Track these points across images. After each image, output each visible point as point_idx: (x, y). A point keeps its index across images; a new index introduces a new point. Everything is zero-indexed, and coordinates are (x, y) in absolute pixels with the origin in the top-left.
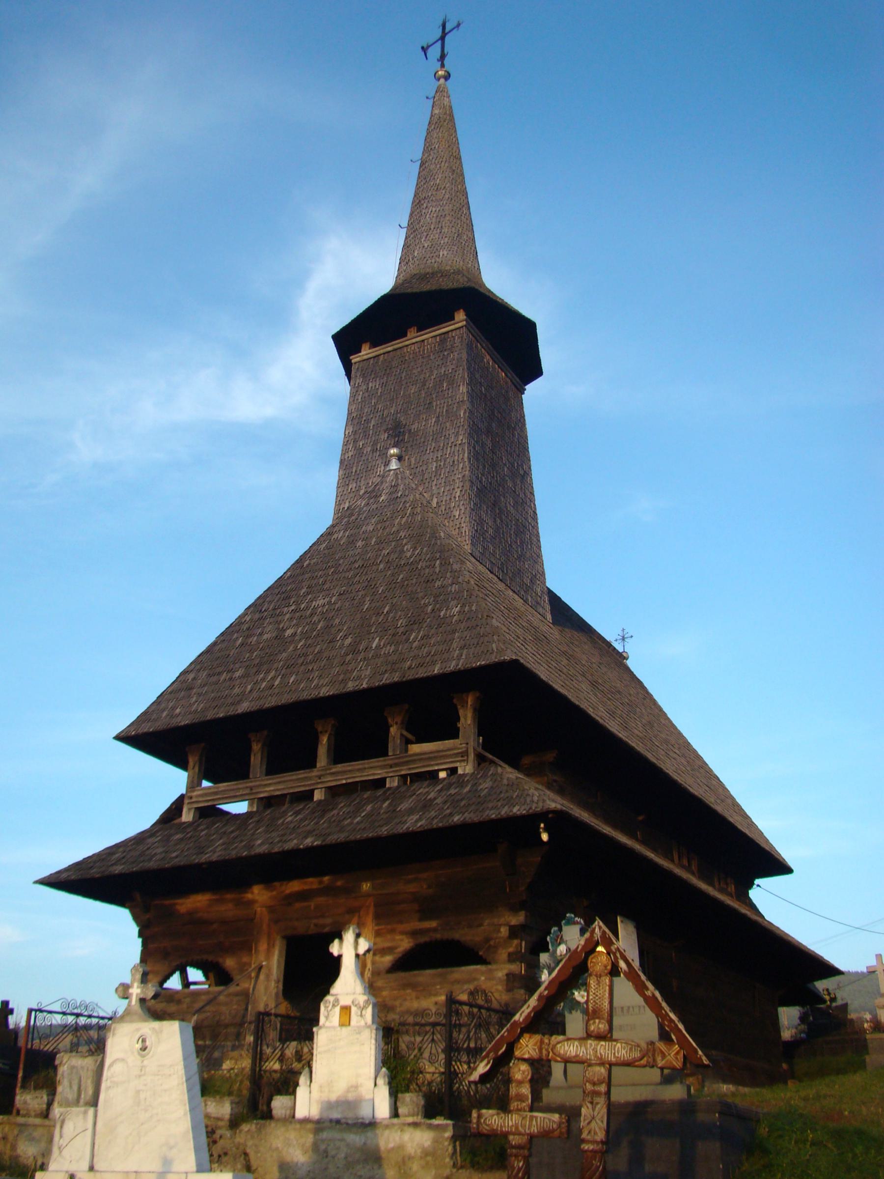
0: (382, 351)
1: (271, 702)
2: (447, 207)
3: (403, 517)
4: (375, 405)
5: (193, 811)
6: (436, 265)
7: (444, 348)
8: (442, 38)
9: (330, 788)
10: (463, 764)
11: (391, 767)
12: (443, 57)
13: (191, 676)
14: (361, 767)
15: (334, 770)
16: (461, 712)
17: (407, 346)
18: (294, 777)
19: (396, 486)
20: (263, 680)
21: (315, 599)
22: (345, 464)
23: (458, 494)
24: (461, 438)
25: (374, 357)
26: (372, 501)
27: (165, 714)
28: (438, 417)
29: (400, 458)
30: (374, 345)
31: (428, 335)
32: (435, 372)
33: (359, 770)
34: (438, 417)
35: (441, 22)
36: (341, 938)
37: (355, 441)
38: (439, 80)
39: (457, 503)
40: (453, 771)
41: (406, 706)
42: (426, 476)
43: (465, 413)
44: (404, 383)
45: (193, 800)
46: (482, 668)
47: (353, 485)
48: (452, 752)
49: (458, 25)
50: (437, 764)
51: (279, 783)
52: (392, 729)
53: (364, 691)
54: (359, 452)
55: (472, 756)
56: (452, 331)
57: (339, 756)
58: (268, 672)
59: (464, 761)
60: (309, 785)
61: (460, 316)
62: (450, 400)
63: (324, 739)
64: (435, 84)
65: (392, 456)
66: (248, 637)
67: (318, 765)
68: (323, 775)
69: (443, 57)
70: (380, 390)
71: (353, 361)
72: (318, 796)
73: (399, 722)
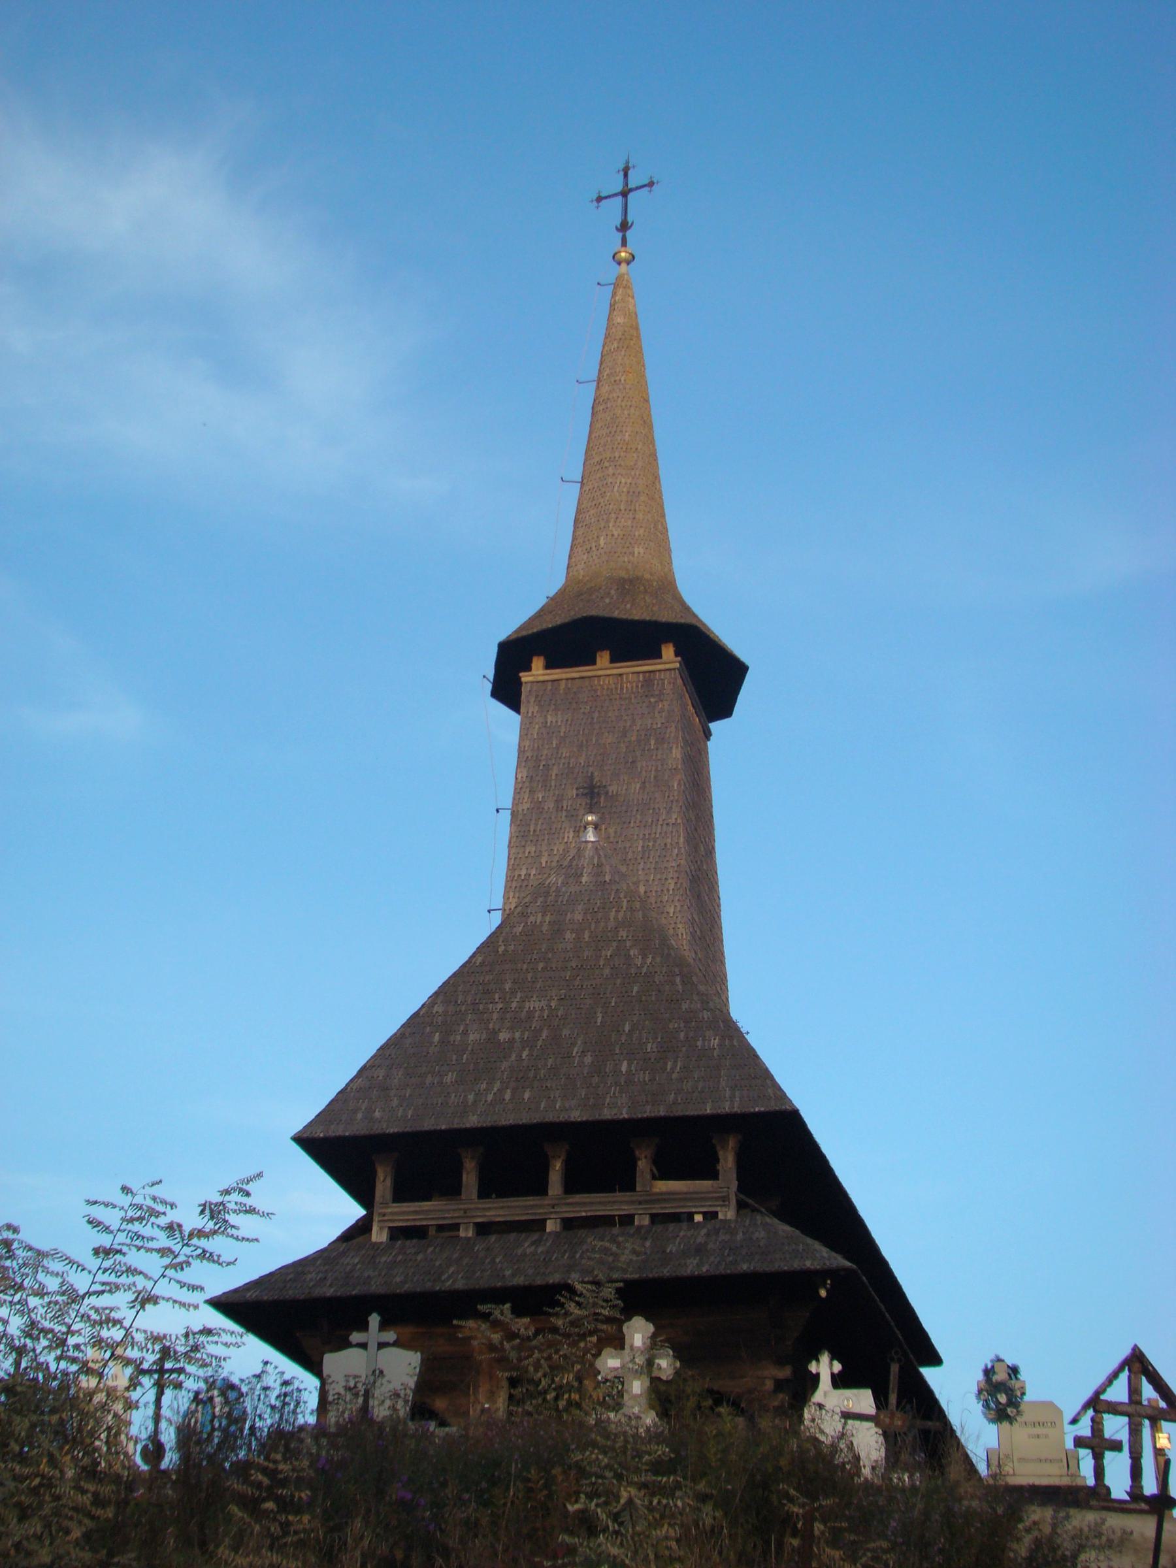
0: (564, 676)
1: (508, 1119)
4: (558, 748)
6: (630, 567)
7: (620, 661)
8: (625, 194)
9: (563, 1219)
10: (724, 1209)
11: (640, 1203)
12: (624, 227)
13: (381, 1073)
15: (571, 1200)
16: (721, 1154)
17: (599, 676)
18: (521, 1204)
19: (600, 865)
22: (519, 819)
23: (672, 886)
24: (674, 816)
25: (553, 681)
26: (571, 880)
27: (360, 1116)
29: (596, 827)
30: (548, 666)
31: (632, 670)
32: (639, 722)
33: (600, 1203)
35: (622, 166)
36: (818, 1361)
38: (619, 263)
40: (710, 1216)
42: (630, 855)
43: (679, 784)
44: (597, 726)
46: (759, 1114)
49: (651, 184)
50: (695, 1207)
51: (502, 1208)
52: (640, 1163)
53: (625, 1121)
54: (538, 807)
57: (572, 1186)
61: (668, 652)
63: (557, 1166)
64: (612, 272)
65: (588, 823)
67: (550, 1192)
68: (555, 1205)
69: (624, 227)
70: (563, 730)
71: (523, 680)
72: (551, 1226)
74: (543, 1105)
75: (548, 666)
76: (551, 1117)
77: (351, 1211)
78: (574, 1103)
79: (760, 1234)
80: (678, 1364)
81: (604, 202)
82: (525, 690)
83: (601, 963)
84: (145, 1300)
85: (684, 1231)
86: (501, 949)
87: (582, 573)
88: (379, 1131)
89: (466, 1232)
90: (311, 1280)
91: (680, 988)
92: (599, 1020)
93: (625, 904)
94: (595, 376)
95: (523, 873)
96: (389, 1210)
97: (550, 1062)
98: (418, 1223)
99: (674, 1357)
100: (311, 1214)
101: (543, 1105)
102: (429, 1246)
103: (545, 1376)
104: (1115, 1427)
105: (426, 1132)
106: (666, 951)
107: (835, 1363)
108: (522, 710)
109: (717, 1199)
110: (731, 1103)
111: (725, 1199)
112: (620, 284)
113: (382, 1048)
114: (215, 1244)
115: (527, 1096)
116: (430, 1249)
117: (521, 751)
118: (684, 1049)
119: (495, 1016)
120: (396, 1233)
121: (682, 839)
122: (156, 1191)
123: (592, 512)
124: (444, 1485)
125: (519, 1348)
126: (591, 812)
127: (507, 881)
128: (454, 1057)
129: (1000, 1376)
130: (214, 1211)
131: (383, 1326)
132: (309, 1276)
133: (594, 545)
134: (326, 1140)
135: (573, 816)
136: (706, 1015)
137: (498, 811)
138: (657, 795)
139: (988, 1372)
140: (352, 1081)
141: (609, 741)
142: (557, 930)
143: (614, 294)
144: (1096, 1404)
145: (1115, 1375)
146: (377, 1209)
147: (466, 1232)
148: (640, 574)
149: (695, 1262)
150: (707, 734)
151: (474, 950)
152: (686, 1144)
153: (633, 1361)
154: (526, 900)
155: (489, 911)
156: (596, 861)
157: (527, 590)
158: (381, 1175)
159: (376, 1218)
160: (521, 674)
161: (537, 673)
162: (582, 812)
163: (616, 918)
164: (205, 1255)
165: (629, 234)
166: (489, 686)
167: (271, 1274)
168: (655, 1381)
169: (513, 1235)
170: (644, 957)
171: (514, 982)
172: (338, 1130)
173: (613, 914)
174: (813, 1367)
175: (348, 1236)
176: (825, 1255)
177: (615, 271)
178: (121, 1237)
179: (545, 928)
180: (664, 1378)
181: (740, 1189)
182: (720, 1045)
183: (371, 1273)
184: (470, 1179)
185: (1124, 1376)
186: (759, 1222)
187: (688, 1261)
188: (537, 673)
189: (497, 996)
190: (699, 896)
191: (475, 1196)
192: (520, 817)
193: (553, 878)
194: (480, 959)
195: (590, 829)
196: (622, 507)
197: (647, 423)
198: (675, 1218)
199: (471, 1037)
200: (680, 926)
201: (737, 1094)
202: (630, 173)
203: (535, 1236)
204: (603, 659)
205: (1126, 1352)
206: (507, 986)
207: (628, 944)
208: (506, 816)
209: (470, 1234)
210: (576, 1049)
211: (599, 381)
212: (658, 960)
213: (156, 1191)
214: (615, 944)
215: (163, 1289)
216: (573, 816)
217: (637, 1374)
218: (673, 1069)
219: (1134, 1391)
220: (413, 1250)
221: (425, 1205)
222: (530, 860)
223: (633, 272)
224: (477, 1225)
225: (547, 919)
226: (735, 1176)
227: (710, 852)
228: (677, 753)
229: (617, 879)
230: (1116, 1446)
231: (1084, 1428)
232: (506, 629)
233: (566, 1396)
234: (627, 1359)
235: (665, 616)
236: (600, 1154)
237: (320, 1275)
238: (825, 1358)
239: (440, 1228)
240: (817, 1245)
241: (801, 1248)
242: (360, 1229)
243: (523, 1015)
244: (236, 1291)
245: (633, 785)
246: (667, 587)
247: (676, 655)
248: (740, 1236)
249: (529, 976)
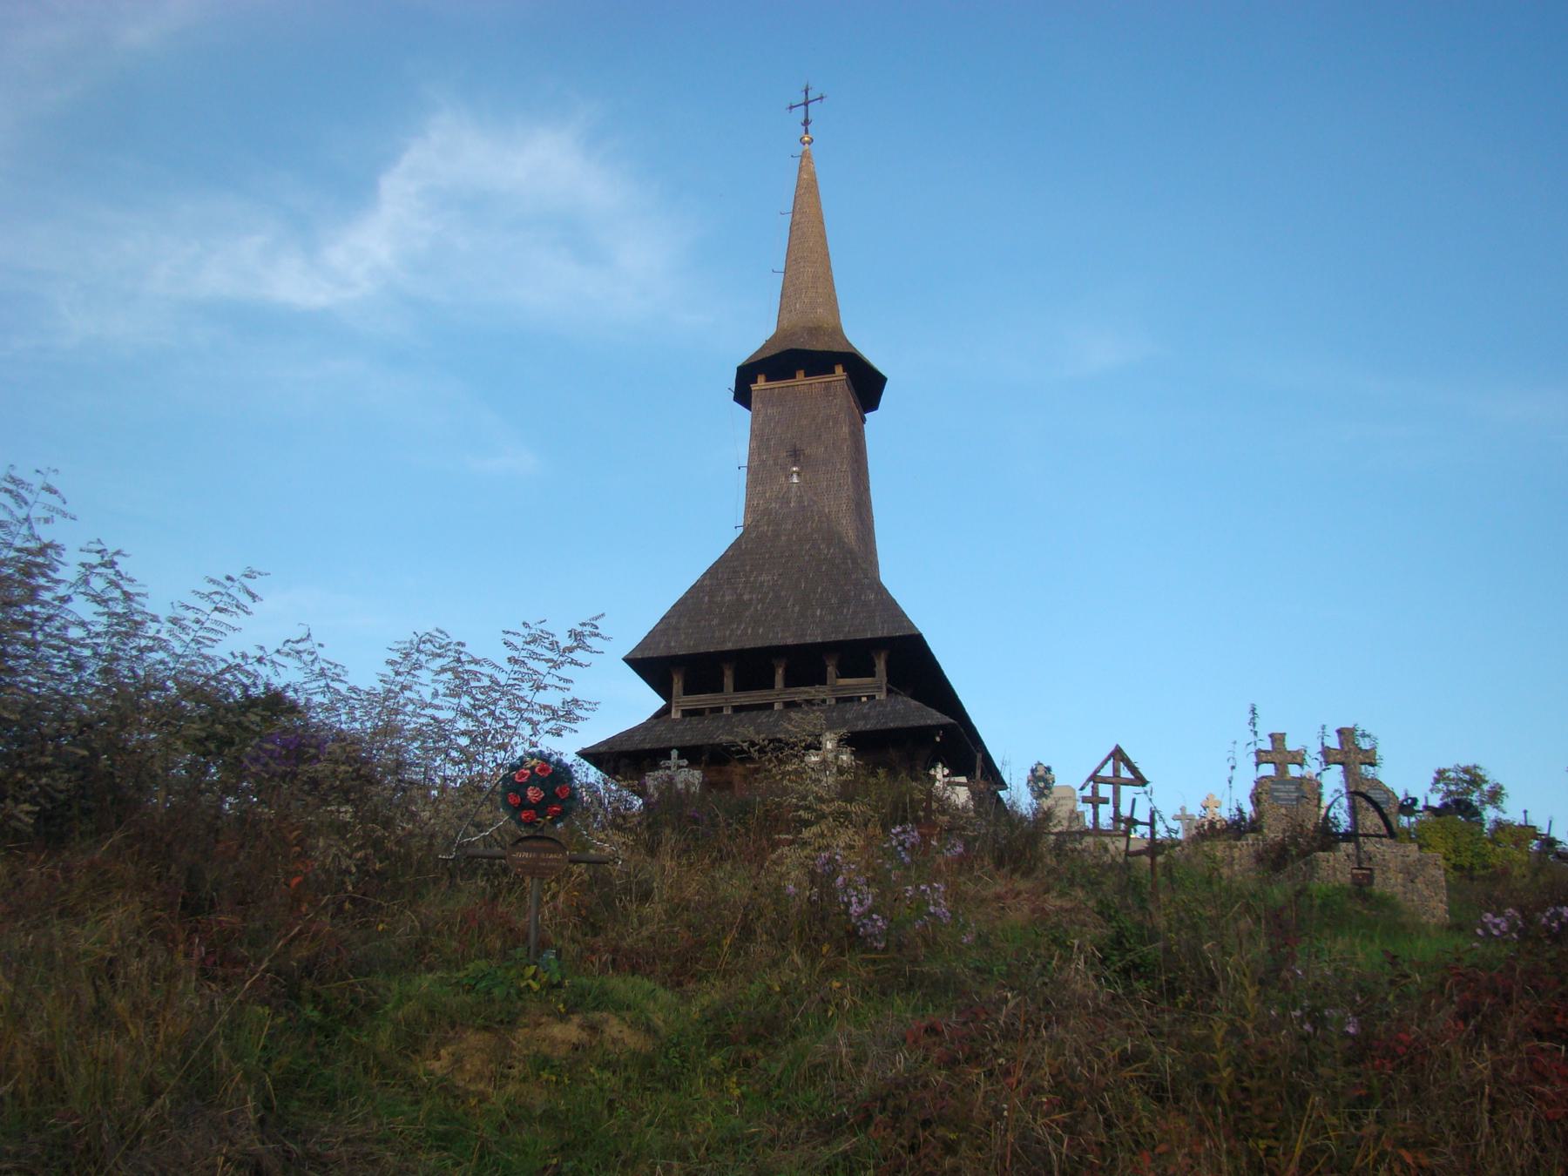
7: (811, 379)
8: (806, 104)
12: (806, 123)
13: (674, 621)
30: (767, 380)
31: (816, 380)
47: (760, 488)
54: (763, 462)
57: (789, 683)
61: (839, 370)
63: (780, 671)
64: (800, 149)
68: (779, 693)
69: (806, 123)
72: (777, 706)
75: (767, 380)
76: (775, 643)
77: (658, 702)
79: (900, 707)
84: (538, 687)
85: (856, 707)
89: (728, 712)
100: (632, 704)
104: (1105, 791)
110: (881, 631)
111: (880, 688)
112: (805, 156)
114: (579, 655)
117: (752, 431)
120: (686, 713)
122: (542, 626)
125: (759, 751)
129: (1041, 772)
130: (576, 635)
135: (784, 468)
139: (1033, 771)
144: (1095, 778)
145: (1105, 762)
147: (728, 712)
150: (864, 420)
152: (854, 657)
157: (754, 332)
161: (761, 384)
164: (573, 662)
172: (648, 654)
178: (524, 653)
184: (728, 681)
185: (1110, 763)
188: (761, 384)
197: (823, 236)
198: (850, 699)
204: (800, 375)
205: (1112, 748)
213: (542, 626)
215: (548, 680)
216: (784, 468)
219: (1116, 770)
221: (702, 696)
227: (867, 489)
228: (846, 429)
230: (1105, 801)
231: (1088, 792)
235: (836, 349)
236: (806, 664)
239: (713, 710)
240: (934, 711)
246: (837, 331)
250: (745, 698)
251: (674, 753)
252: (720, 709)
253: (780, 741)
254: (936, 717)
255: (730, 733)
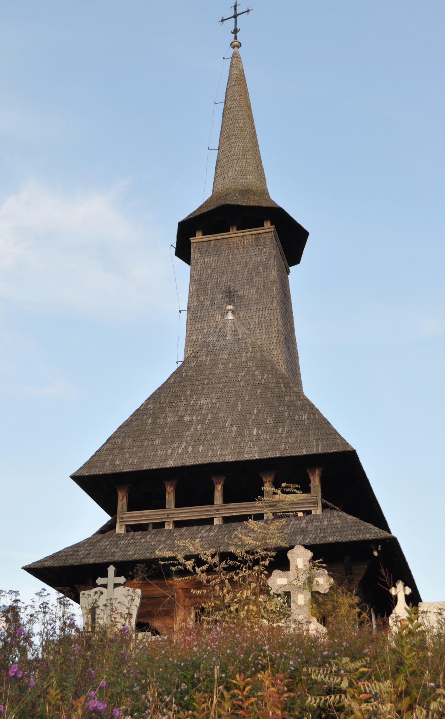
0: (213, 238)
2: (249, 145)
3: (247, 353)
5: (124, 526)
6: (245, 185)
7: (241, 229)
8: (235, 17)
10: (315, 508)
12: (236, 31)
13: (119, 441)
14: (246, 506)
16: (312, 478)
17: (231, 238)
18: (199, 509)
20: (179, 447)
21: (200, 398)
24: (275, 305)
25: (207, 241)
26: (220, 339)
27: (107, 464)
28: (258, 289)
29: (233, 312)
30: (204, 234)
32: (254, 259)
34: (258, 289)
35: (233, 5)
36: (395, 587)
37: (198, 296)
39: (275, 347)
41: (275, 472)
42: (252, 326)
43: (276, 289)
45: (124, 520)
46: (334, 453)
48: (307, 501)
53: (256, 460)
54: (202, 304)
55: (320, 505)
56: (263, 233)
57: (228, 498)
58: (181, 443)
59: (316, 507)
60: (210, 515)
61: (268, 226)
62: (265, 279)
65: (229, 310)
66: (156, 418)
68: (219, 508)
69: (236, 31)
71: (192, 241)
72: (217, 522)
73: (271, 481)
74: (210, 454)
76: (215, 460)
77: (104, 518)
78: (227, 452)
79: (337, 521)
80: (332, 581)
81: (225, 22)
82: (193, 246)
83: (239, 379)
86: (184, 375)
87: (220, 189)
88: (119, 471)
89: (169, 527)
90: (82, 554)
91: (284, 390)
92: (239, 408)
93: (250, 349)
94: (224, 101)
95: (195, 338)
96: (125, 516)
97: (213, 431)
98: (141, 522)
99: (329, 575)
100: (82, 520)
101: (210, 454)
102: (148, 534)
103: (228, 593)
105: (145, 471)
106: (274, 372)
107: (407, 588)
108: (192, 261)
109: (310, 503)
111: (315, 503)
112: (236, 58)
113: (120, 427)
115: (200, 449)
116: (149, 536)
118: (288, 421)
119: (182, 408)
121: (279, 317)
123: (225, 160)
124: (144, 688)
126: (230, 304)
127: (186, 342)
128: (160, 431)
131: (117, 574)
132: (81, 553)
133: (226, 175)
134: (89, 477)
135: (220, 308)
136: (299, 403)
137: (180, 312)
138: (265, 295)
140: (103, 445)
141: (238, 269)
142: (214, 364)
143: (232, 61)
146: (119, 516)
147: (169, 527)
148: (251, 188)
149: (301, 537)
150: (288, 272)
151: (169, 376)
152: (291, 471)
153: (297, 579)
154: (197, 349)
155: (177, 363)
156: (233, 329)
157: (196, 195)
158: (120, 497)
159: (118, 520)
160: (191, 239)
162: (225, 305)
163: (246, 356)
165: (238, 34)
166: (174, 250)
167: (60, 552)
168: (315, 595)
169: (195, 528)
170: (263, 375)
171: (192, 391)
173: (244, 354)
174: (393, 591)
175: (103, 531)
176: (378, 531)
177: (232, 51)
179: (207, 363)
180: (322, 592)
181: (323, 497)
182: (308, 418)
183: (115, 550)
184: (170, 497)
186: (336, 515)
187: (297, 538)
189: (182, 398)
190: (289, 348)
191: (173, 506)
192: (192, 310)
193: (211, 338)
194: (172, 380)
195: (230, 314)
196: (240, 157)
199: (169, 420)
200: (280, 361)
201: (320, 443)
202: (237, 7)
203: (208, 527)
206: (188, 393)
207: (253, 369)
208: (184, 315)
209: (171, 528)
210: (227, 424)
211: (225, 102)
212: (270, 376)
214: (246, 369)
216: (220, 308)
217: (301, 589)
218: (283, 430)
220: (139, 537)
222: (198, 331)
223: (240, 51)
224: (175, 522)
225: (209, 358)
226: (320, 489)
229: (245, 337)
232: (183, 216)
233: (246, 608)
234: (292, 578)
235: (265, 204)
236: (243, 480)
237: (87, 552)
238: (400, 585)
240: (371, 526)
241: (362, 527)
242: (109, 528)
243: (197, 407)
244: (39, 562)
245: (252, 291)
246: (265, 193)
247: (271, 225)
248: (326, 523)
249: (200, 387)
250: (187, 513)
251: (111, 570)
252: (161, 525)
253: (233, 557)
254: (372, 532)
255: (171, 549)
